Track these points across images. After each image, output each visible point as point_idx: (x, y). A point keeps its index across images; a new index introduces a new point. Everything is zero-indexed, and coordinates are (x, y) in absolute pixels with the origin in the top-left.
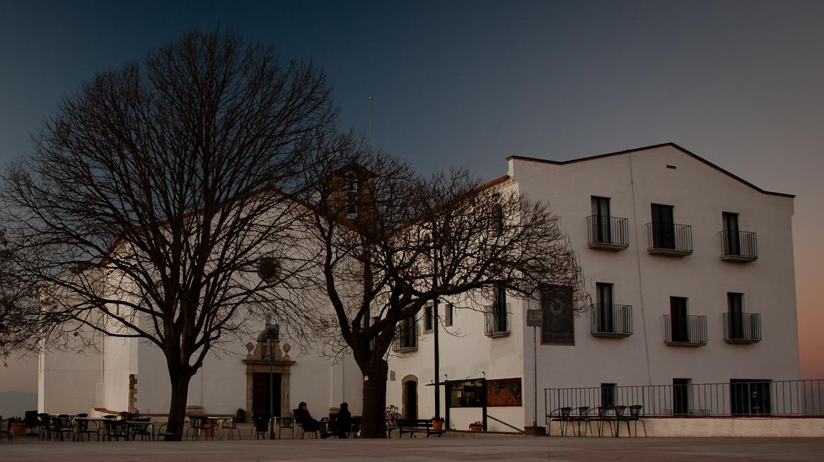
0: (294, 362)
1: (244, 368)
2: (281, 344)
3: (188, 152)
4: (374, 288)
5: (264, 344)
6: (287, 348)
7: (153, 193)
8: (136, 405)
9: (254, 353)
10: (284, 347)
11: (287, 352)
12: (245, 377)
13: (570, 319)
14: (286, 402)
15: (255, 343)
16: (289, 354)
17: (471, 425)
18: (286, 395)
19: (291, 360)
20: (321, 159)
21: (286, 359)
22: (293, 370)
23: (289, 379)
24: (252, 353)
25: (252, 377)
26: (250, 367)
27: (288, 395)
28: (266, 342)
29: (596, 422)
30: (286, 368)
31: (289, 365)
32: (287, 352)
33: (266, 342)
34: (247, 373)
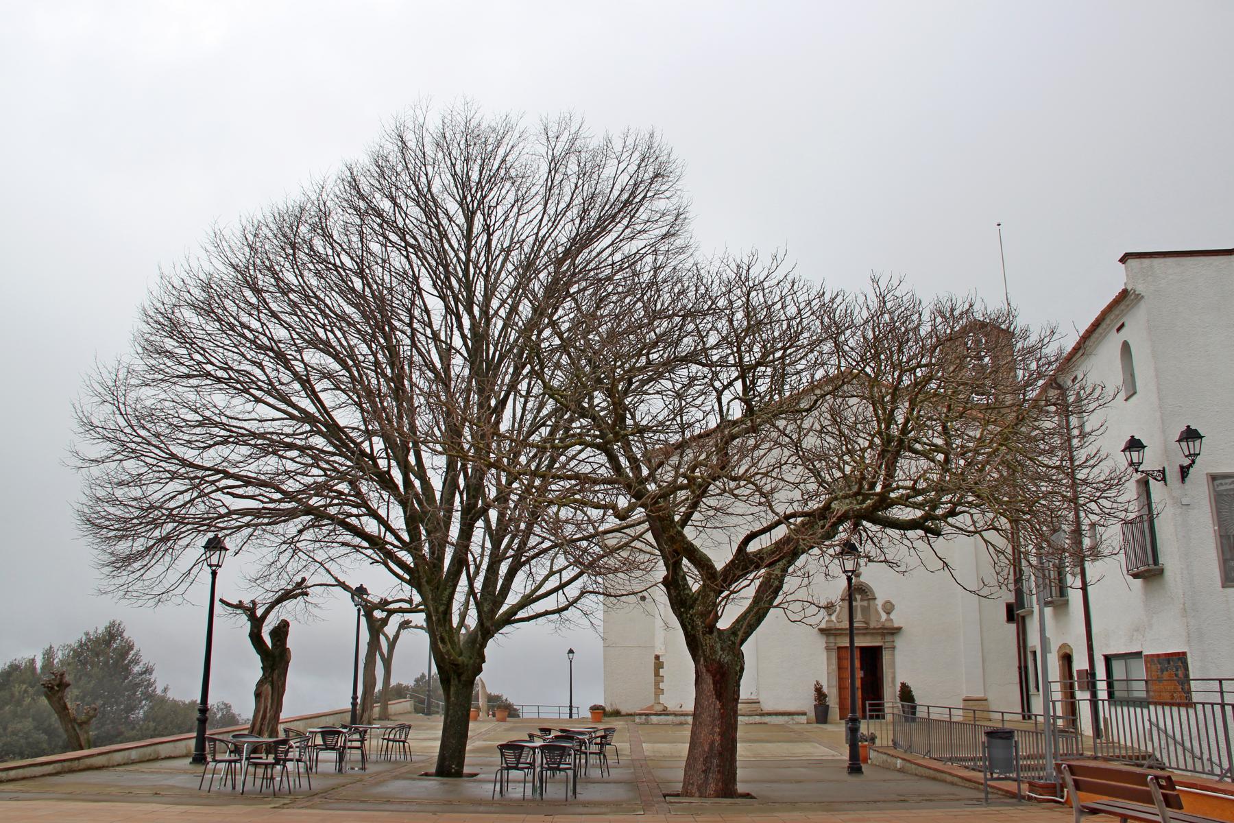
0: (899, 629)
1: (821, 642)
2: (879, 602)
3: (382, 463)
4: (524, 559)
6: (889, 608)
7: (457, 495)
8: (662, 699)
9: (837, 617)
10: (884, 606)
11: (888, 613)
12: (824, 655)
13: (726, 658)
16: (892, 616)
19: (896, 625)
20: (1034, 434)
21: (888, 625)
22: (900, 642)
24: (833, 618)
25: (834, 655)
26: (832, 639)
32: (888, 613)
34: (828, 649)
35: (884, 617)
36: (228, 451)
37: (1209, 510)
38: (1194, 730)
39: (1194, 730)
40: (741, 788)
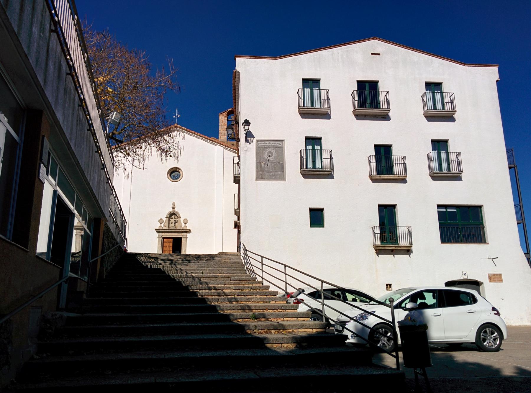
2: (182, 219)
15: (164, 219)
16: (187, 225)
21: (185, 228)
24: (162, 225)
35: (183, 225)
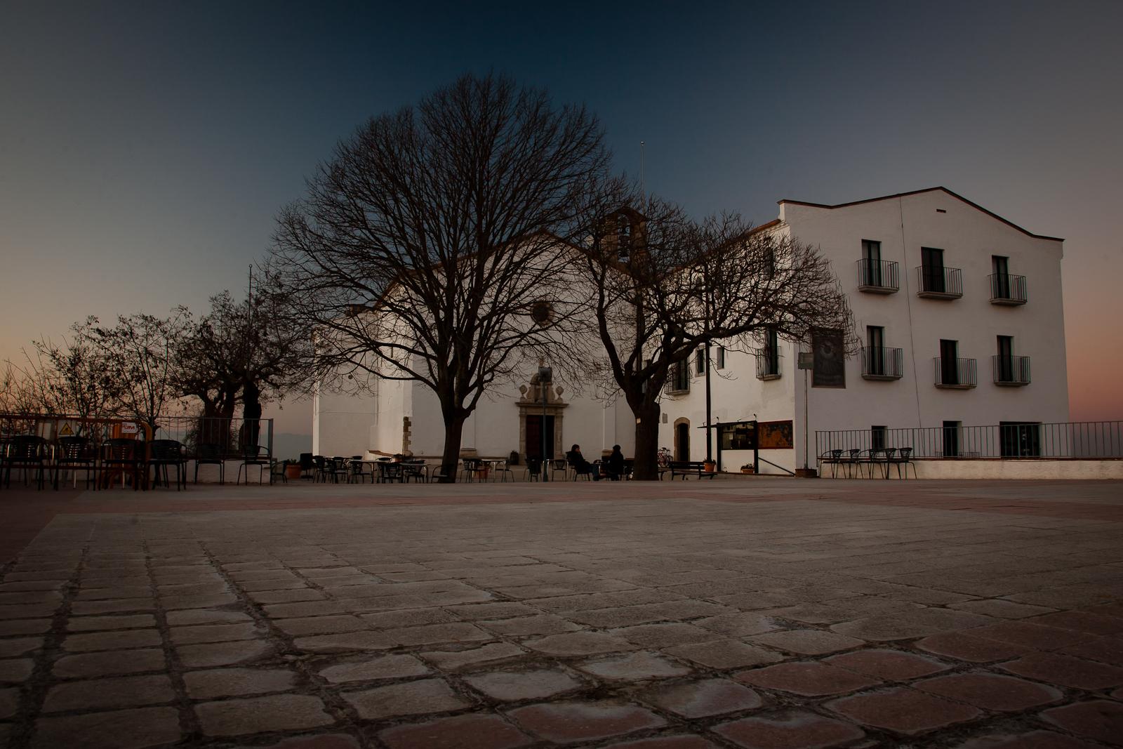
0: (567, 405)
1: (517, 410)
2: (554, 387)
4: (646, 331)
5: (538, 387)
6: (560, 391)
8: (410, 447)
9: (528, 396)
10: (557, 390)
11: (559, 395)
12: (518, 420)
14: (559, 444)
16: (561, 396)
17: (743, 468)
18: (559, 438)
19: (564, 403)
21: (559, 402)
23: (562, 422)
24: (525, 395)
26: (524, 410)
27: (561, 437)
28: (539, 385)
29: (867, 464)
30: (559, 411)
31: (562, 408)
32: (559, 395)
33: (539, 385)
34: (521, 416)
36: (531, 143)
37: (1032, 374)
38: (932, 440)
39: (932, 440)
40: (760, 472)
